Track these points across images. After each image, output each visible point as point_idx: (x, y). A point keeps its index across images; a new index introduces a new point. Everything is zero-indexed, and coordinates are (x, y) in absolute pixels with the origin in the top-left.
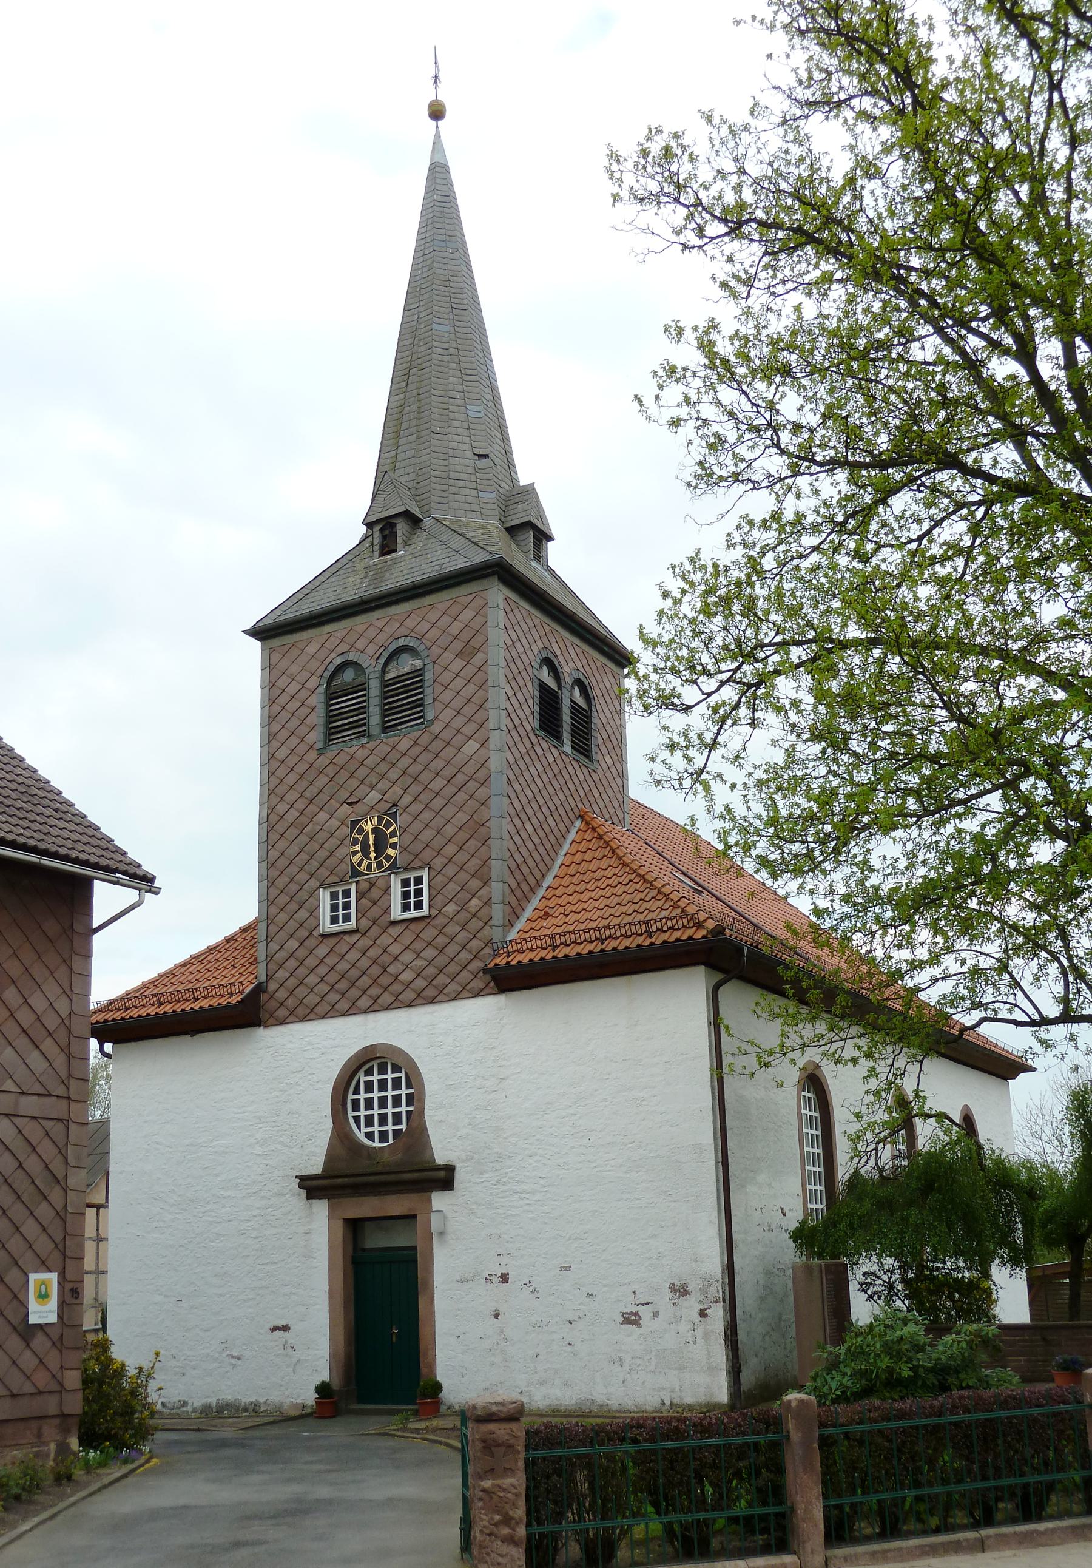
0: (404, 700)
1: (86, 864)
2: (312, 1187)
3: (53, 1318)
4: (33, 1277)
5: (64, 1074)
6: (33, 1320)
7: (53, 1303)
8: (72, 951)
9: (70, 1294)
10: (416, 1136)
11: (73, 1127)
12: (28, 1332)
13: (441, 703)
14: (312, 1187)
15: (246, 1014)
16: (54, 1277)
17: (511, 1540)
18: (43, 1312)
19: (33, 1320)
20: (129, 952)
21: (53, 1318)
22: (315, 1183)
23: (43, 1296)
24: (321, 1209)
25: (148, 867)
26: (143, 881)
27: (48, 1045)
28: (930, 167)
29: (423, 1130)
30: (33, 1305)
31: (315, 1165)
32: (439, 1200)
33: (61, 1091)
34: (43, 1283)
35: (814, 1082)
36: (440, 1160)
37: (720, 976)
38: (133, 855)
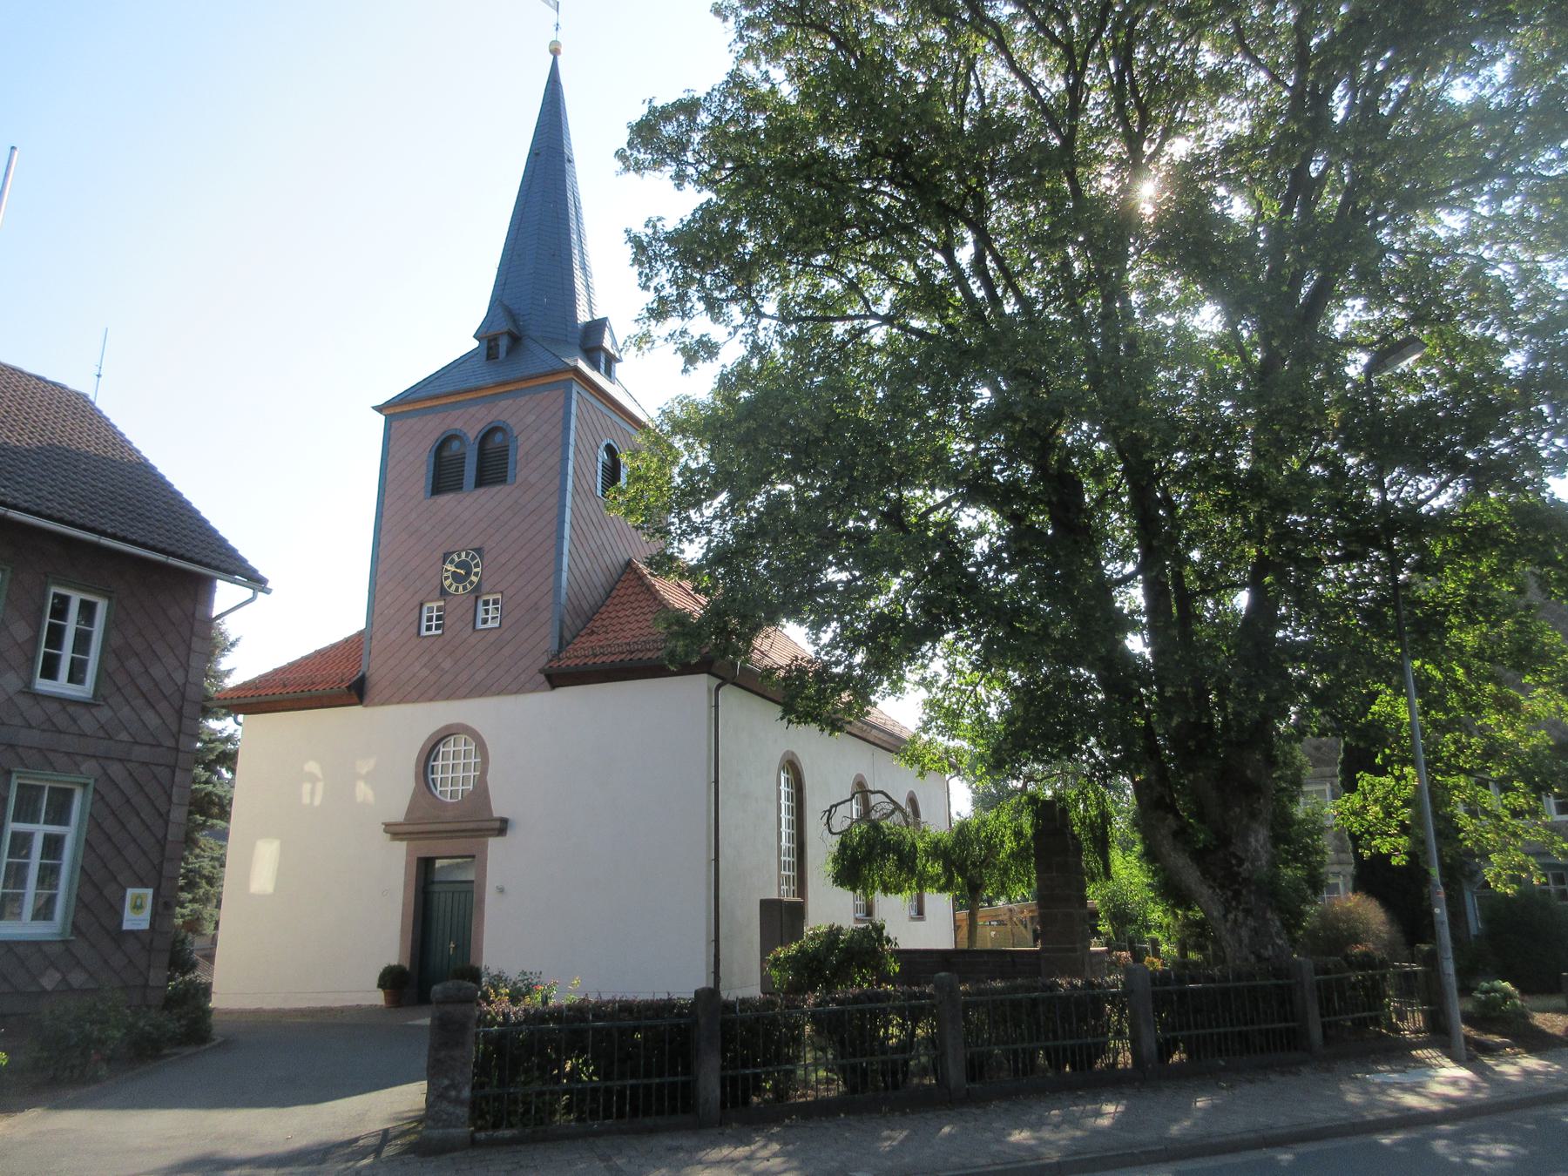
0: (493, 464)
1: (208, 565)
2: (395, 831)
3: (145, 926)
4: (130, 892)
5: (174, 728)
6: (126, 926)
7: (147, 913)
8: (192, 633)
9: (163, 907)
10: (481, 792)
11: (178, 772)
12: (120, 936)
13: (526, 466)
14: (395, 831)
15: (357, 692)
16: (149, 892)
17: (458, 1101)
18: (136, 919)
19: (126, 926)
20: (256, 636)
21: (145, 926)
22: (399, 829)
23: (137, 907)
24: (401, 847)
25: (262, 572)
26: (256, 582)
27: (163, 706)
28: (938, 128)
29: (486, 790)
30: (128, 913)
31: (398, 813)
32: (494, 844)
33: (170, 743)
34: (139, 896)
35: (792, 767)
36: (496, 814)
37: (718, 681)
38: (253, 562)
